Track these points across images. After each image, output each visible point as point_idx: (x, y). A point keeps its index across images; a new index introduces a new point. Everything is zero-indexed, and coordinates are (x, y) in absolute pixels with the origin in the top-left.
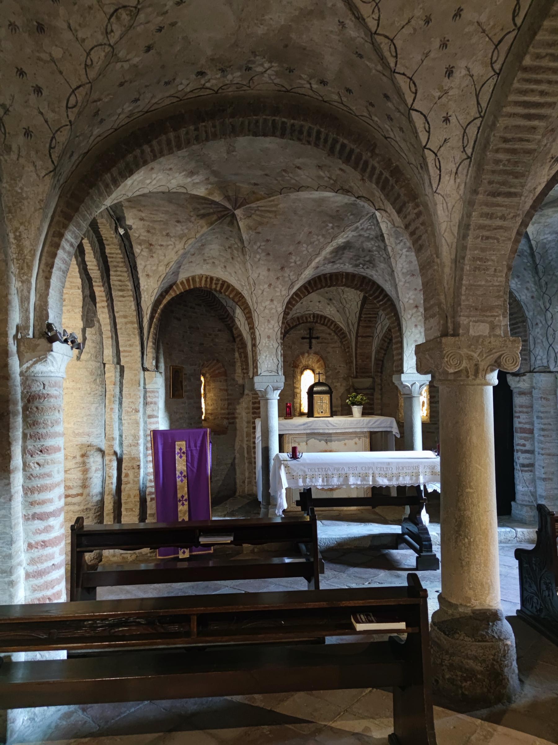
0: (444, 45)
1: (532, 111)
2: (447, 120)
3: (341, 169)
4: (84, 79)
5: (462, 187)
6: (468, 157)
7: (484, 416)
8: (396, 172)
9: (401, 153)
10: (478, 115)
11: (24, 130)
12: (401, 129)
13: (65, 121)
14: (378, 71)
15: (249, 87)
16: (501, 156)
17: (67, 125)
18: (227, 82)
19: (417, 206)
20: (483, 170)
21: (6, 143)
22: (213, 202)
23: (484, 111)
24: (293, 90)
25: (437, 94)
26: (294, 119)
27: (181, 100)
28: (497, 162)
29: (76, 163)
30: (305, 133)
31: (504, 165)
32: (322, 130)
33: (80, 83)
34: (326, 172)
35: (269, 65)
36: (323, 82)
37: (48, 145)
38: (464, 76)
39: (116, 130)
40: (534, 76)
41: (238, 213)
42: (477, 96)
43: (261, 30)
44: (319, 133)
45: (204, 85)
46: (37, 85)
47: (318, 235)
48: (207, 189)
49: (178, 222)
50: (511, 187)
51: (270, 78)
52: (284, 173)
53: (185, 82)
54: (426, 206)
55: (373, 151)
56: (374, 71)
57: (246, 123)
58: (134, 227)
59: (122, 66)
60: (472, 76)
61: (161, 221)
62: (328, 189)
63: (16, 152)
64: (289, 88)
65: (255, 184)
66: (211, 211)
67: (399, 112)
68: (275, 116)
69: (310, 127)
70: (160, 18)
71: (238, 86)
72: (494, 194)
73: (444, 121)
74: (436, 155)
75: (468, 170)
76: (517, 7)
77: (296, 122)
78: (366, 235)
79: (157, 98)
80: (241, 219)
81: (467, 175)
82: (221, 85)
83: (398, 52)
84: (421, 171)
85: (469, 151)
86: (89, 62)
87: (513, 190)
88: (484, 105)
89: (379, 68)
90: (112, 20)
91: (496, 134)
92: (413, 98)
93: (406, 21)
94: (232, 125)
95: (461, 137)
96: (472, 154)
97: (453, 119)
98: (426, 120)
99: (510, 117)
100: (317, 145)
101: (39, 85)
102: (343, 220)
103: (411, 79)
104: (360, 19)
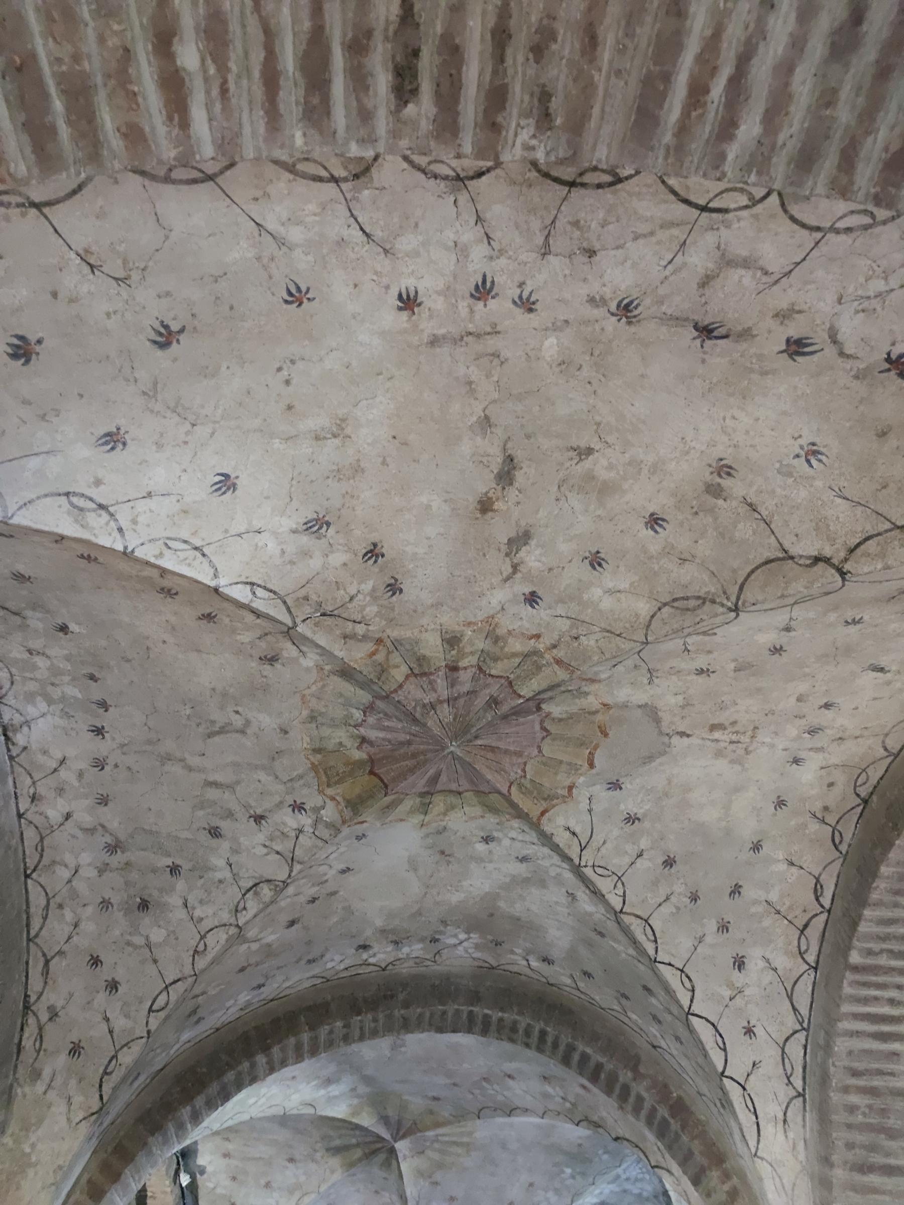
0: (724, 927)
1: (886, 1028)
2: (749, 1031)
3: (584, 1087)
4: (188, 970)
5: (801, 1146)
6: (799, 1095)
7: (682, 50)
8: (680, 1108)
9: (685, 1076)
10: (798, 1027)
11: (72, 1045)
12: (678, 1039)
13: (141, 1031)
14: (630, 955)
15: (435, 962)
16: (854, 1099)
17: (142, 1037)
18: (401, 956)
19: (726, 1176)
20: (831, 1122)
21: (36, 1065)
22: (358, 1127)
23: (806, 1021)
24: (502, 967)
25: (727, 993)
26: (502, 1010)
27: (328, 981)
28: (852, 1109)
29: (139, 1090)
30: (521, 1032)
31: (864, 1114)
32: (549, 1029)
33: (179, 976)
34: (558, 1089)
35: (466, 936)
36: (546, 960)
37: (101, 1070)
38: (762, 970)
39: (218, 1030)
40: (874, 979)
41: (402, 1147)
42: (790, 998)
43: (455, 898)
44: (543, 1034)
45: (366, 960)
46: (113, 979)
47: (546, 1190)
48: (351, 1105)
49: (291, 1160)
50: (888, 1155)
51: (466, 951)
52: (484, 1084)
53: (338, 958)
54: (743, 1177)
55: (635, 1069)
56: (624, 955)
57: (428, 1014)
58: (209, 1169)
59: (249, 948)
60: (775, 970)
61: (260, 1158)
62: (561, 1116)
63: (47, 1080)
64: (494, 964)
65: (436, 1099)
66: (354, 1141)
67: (671, 1013)
68: (472, 1005)
69: (529, 1025)
70: (316, 888)
71: (417, 960)
72: (864, 1168)
73: (745, 1034)
74: (744, 1089)
75: (804, 1116)
76: (819, 887)
77: (506, 1015)
78: (636, 1191)
79: (294, 980)
80: (405, 1158)
81: (804, 1126)
82: (392, 959)
83: (657, 936)
84: (722, 1110)
85: (798, 1083)
86: (201, 947)
87: (892, 1161)
88: (804, 1012)
89: (631, 951)
90: (247, 896)
91: (837, 1063)
92: (689, 998)
93: (665, 898)
94: (404, 1018)
95: (779, 1059)
96: (804, 1090)
97: (758, 1030)
98: (717, 1030)
99: (852, 1036)
100: (540, 1050)
101: (117, 979)
102: (591, 1161)
103: (682, 971)
104: (597, 894)
